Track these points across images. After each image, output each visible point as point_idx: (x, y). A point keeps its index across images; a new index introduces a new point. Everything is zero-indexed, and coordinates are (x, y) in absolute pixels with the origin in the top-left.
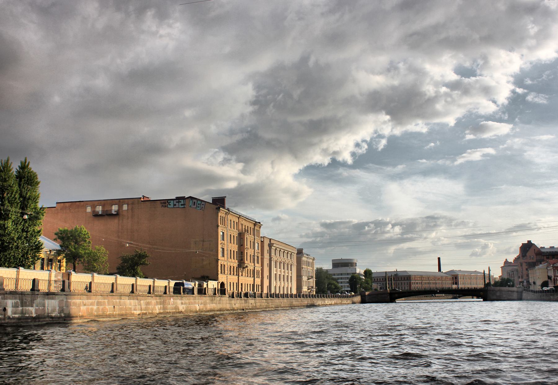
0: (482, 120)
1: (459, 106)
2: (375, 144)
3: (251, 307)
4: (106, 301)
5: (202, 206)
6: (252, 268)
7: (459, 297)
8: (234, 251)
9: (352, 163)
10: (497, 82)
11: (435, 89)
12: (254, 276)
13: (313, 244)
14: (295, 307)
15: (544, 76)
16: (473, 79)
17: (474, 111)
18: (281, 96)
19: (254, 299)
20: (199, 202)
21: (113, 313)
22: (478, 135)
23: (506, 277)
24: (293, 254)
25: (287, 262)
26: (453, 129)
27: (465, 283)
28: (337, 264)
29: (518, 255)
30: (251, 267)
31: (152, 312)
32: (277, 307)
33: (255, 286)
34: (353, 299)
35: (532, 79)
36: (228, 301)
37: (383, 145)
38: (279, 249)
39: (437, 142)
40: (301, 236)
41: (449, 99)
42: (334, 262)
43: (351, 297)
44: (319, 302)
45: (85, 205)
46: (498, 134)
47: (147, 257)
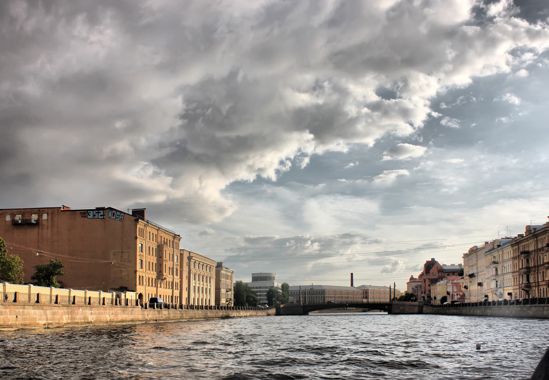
0: (399, 142)
1: (379, 127)
2: (298, 162)
3: (164, 318)
4: (8, 310)
5: (121, 217)
6: (171, 280)
7: (369, 311)
8: (152, 263)
9: (276, 180)
10: (415, 105)
11: (357, 110)
12: (172, 288)
13: (230, 259)
14: (209, 318)
15: (458, 101)
16: (393, 101)
17: (392, 133)
18: (210, 110)
19: (168, 310)
20: (118, 213)
21: (16, 323)
22: (394, 157)
23: (410, 292)
24: (212, 267)
25: (202, 273)
26: (372, 150)
27: (374, 297)
28: (256, 278)
29: (422, 272)
30: (169, 279)
31: (59, 322)
32: (191, 319)
33: (174, 298)
34: (268, 312)
35: (447, 104)
36: (140, 313)
37: (306, 163)
39: (356, 162)
40: (226, 250)
41: (370, 120)
43: (266, 309)
44: (234, 314)
45: (4, 213)
46: (413, 156)
47: (62, 267)
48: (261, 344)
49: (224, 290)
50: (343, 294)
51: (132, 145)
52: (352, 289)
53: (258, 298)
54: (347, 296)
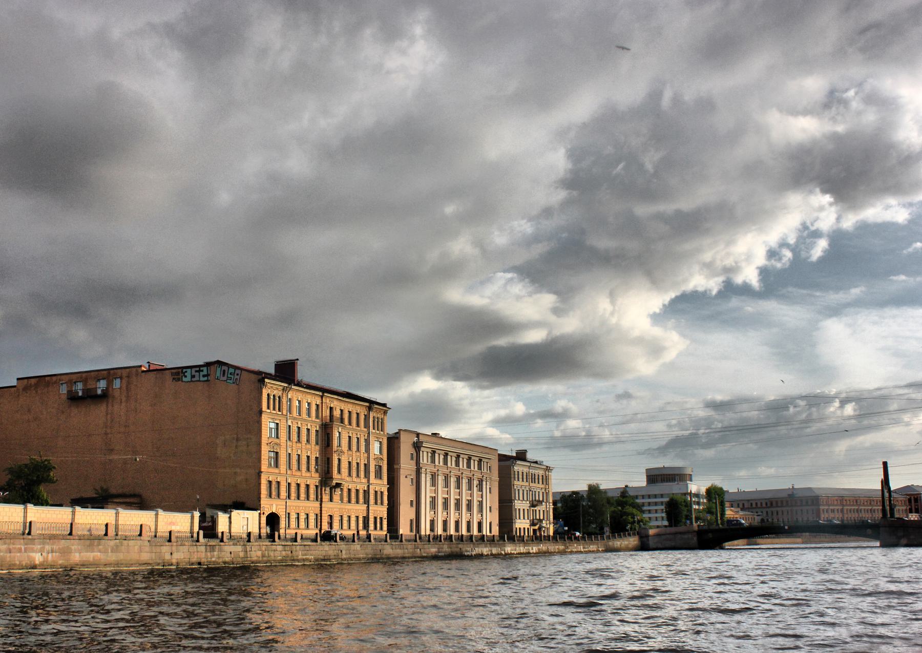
5: (236, 377)
18: (621, 166)
20: (232, 370)
28: (654, 477)
38: (455, 455)
42: (649, 474)
48: (747, 602)
49: (524, 502)
50: (860, 505)
51: (479, 244)
53: (646, 516)
54: (870, 508)
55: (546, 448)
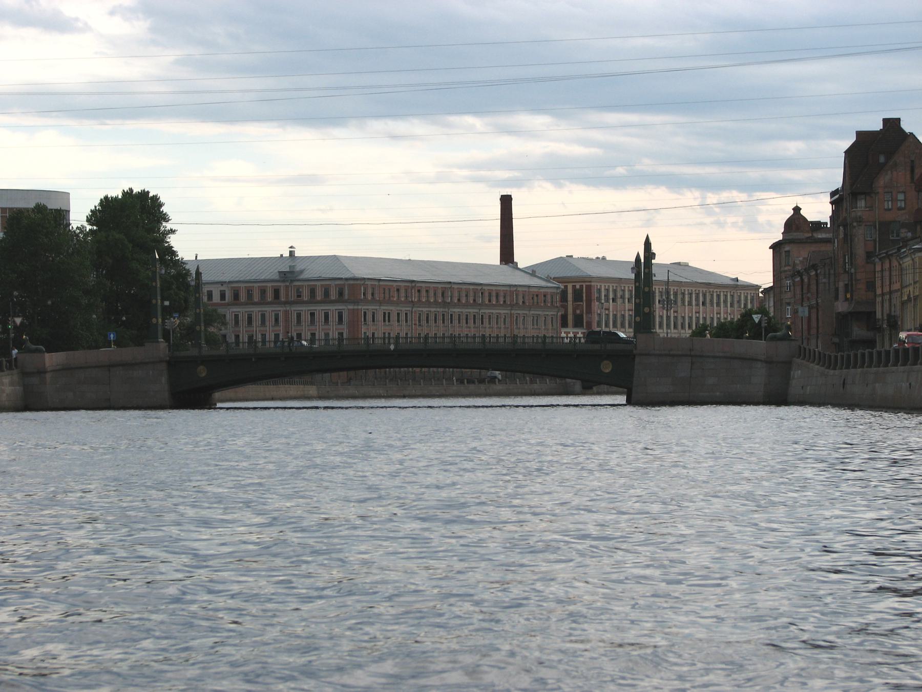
50: (482, 305)
52: (508, 277)
55: (23, 113)
